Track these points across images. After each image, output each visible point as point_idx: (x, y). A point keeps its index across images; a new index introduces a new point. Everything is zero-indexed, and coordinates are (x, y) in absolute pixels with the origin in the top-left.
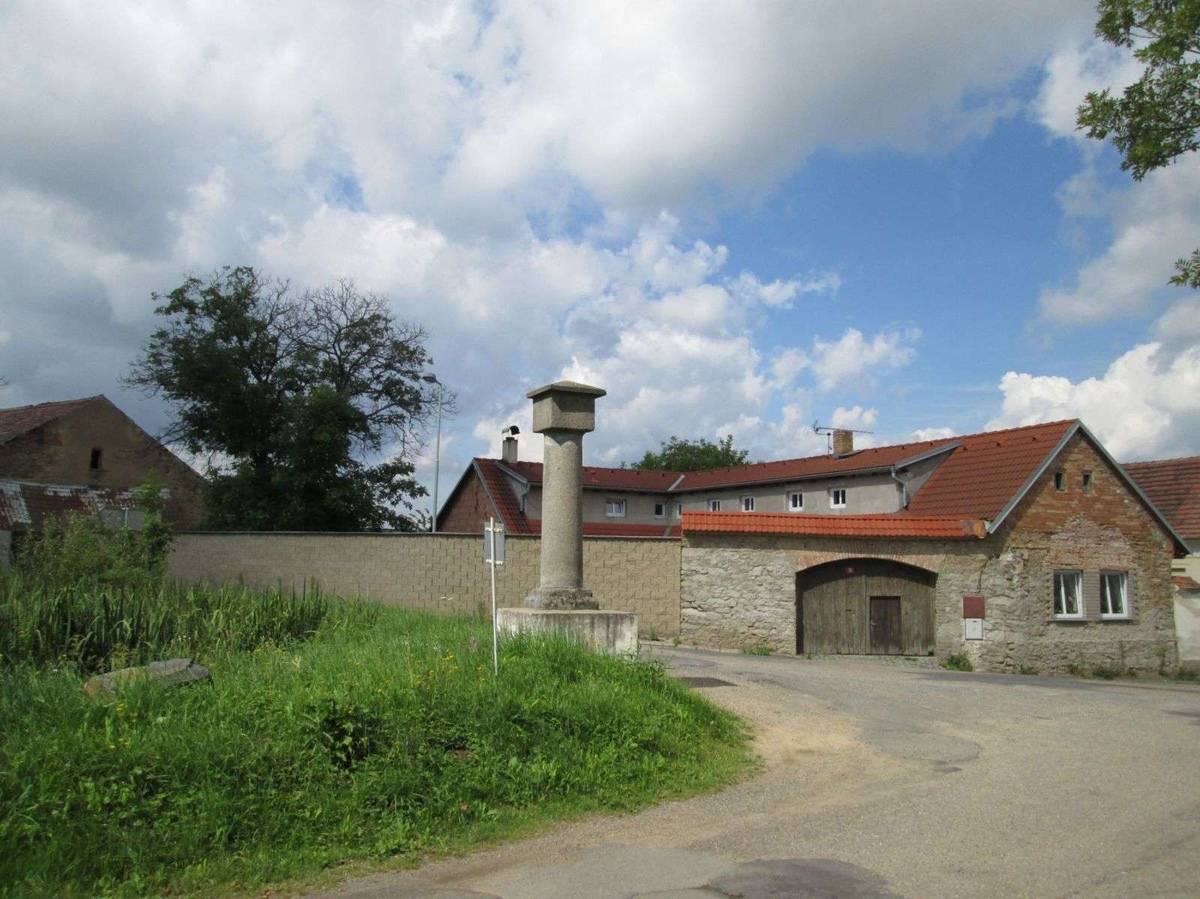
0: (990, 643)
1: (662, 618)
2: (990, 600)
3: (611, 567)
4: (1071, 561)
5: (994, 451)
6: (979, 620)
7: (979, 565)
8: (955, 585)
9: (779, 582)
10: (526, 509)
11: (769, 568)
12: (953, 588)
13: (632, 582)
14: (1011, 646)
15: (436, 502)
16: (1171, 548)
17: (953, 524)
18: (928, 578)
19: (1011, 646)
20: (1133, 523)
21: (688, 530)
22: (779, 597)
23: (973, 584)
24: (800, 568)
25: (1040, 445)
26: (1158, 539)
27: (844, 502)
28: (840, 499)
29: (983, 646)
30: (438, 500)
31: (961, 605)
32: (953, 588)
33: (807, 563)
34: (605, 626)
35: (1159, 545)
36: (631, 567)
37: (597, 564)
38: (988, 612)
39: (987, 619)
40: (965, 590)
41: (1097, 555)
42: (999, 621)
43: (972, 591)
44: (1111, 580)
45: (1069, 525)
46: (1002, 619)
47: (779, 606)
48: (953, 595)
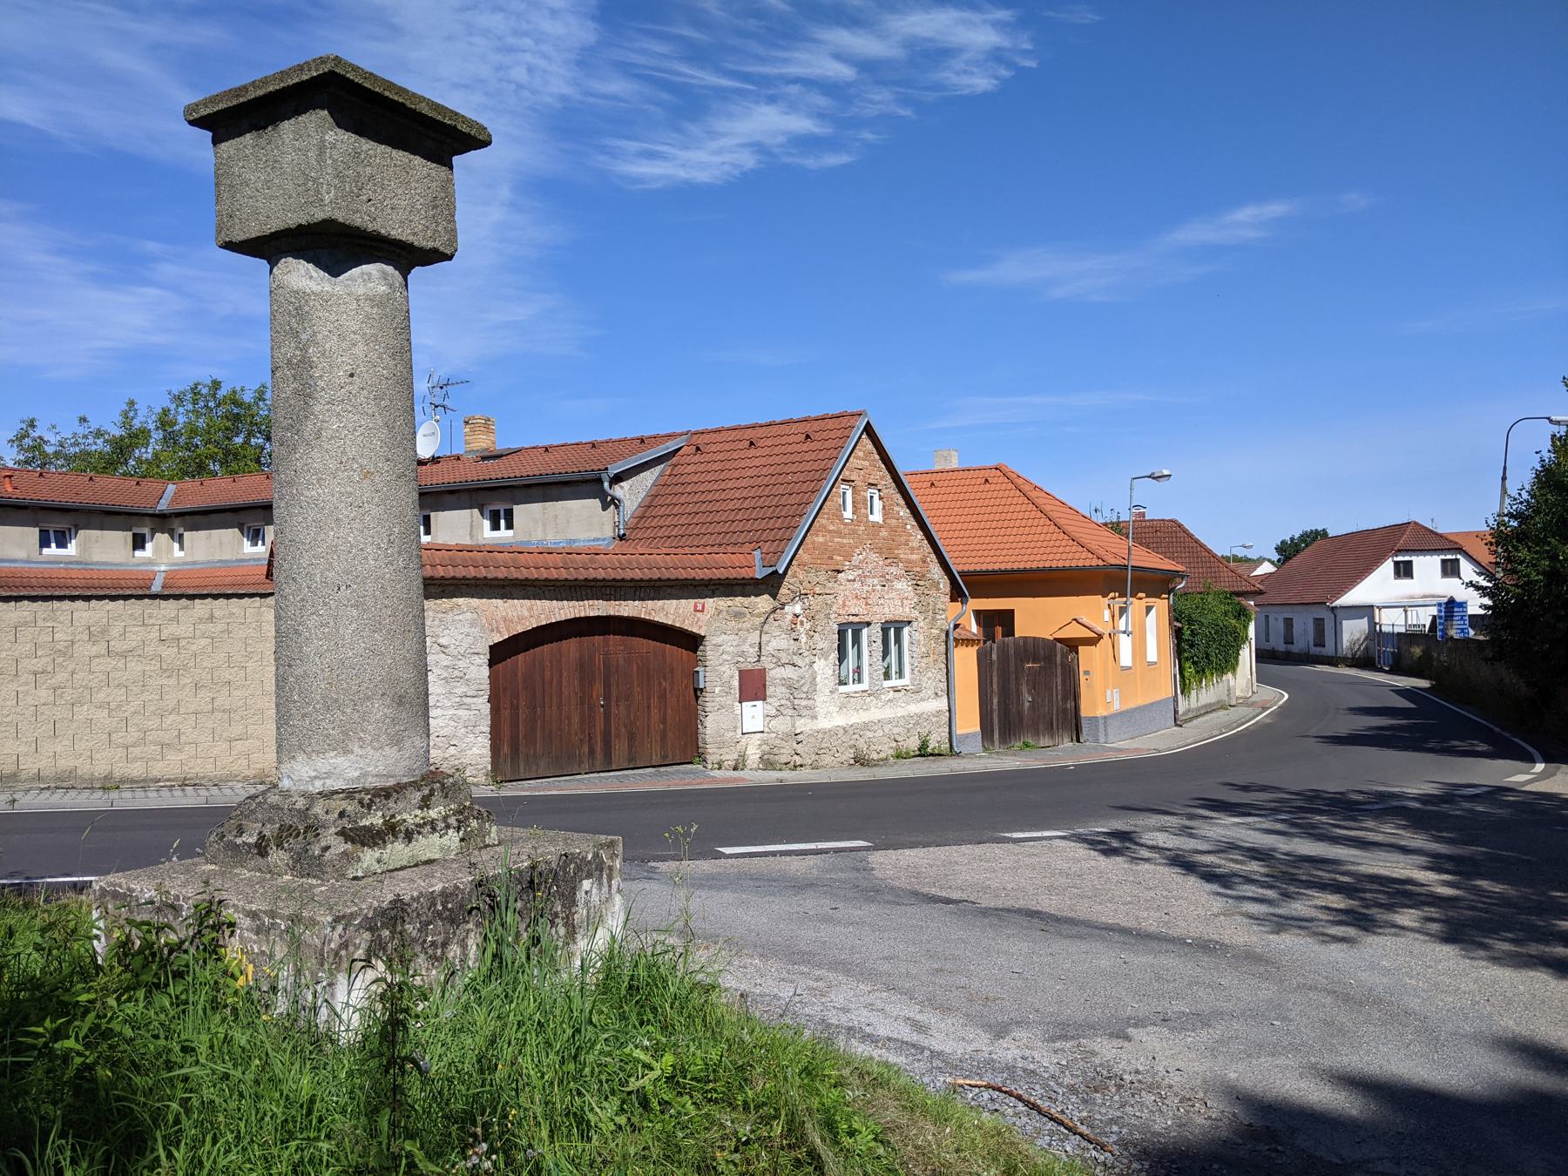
0: (773, 735)
1: (239, 746)
2: (774, 672)
3: (124, 655)
4: (857, 609)
5: (743, 454)
6: (759, 703)
7: (758, 621)
8: (728, 653)
9: (461, 664)
10: (152, 292)
11: (443, 641)
12: (725, 657)
13: (172, 681)
14: (800, 738)
15: (1206, 947)
16: (948, 589)
17: (738, 560)
18: (691, 642)
19: (800, 738)
20: (914, 557)
21: (432, 578)
22: (459, 691)
23: (751, 650)
24: (498, 639)
25: (708, 457)
26: (936, 576)
27: (510, 526)
28: (502, 522)
29: (765, 742)
30: (1193, 929)
31: (736, 683)
32: (725, 657)
33: (508, 631)
34: (347, 976)
35: (936, 585)
36: (168, 652)
37: (94, 650)
38: (770, 691)
39: (769, 700)
40: (741, 659)
41: (882, 601)
42: (783, 702)
43: (749, 664)
44: (893, 629)
45: (856, 559)
46: (788, 699)
47: (460, 705)
48: (725, 668)
